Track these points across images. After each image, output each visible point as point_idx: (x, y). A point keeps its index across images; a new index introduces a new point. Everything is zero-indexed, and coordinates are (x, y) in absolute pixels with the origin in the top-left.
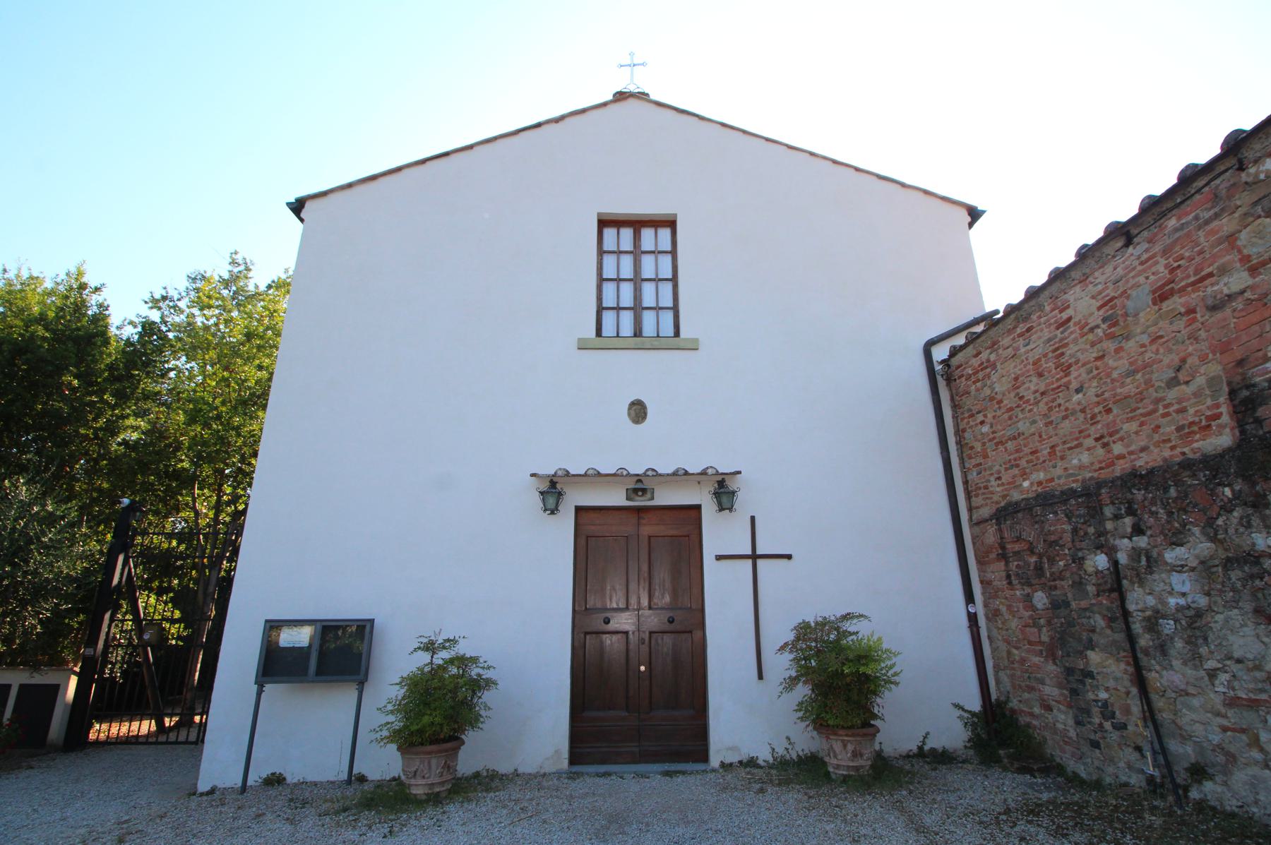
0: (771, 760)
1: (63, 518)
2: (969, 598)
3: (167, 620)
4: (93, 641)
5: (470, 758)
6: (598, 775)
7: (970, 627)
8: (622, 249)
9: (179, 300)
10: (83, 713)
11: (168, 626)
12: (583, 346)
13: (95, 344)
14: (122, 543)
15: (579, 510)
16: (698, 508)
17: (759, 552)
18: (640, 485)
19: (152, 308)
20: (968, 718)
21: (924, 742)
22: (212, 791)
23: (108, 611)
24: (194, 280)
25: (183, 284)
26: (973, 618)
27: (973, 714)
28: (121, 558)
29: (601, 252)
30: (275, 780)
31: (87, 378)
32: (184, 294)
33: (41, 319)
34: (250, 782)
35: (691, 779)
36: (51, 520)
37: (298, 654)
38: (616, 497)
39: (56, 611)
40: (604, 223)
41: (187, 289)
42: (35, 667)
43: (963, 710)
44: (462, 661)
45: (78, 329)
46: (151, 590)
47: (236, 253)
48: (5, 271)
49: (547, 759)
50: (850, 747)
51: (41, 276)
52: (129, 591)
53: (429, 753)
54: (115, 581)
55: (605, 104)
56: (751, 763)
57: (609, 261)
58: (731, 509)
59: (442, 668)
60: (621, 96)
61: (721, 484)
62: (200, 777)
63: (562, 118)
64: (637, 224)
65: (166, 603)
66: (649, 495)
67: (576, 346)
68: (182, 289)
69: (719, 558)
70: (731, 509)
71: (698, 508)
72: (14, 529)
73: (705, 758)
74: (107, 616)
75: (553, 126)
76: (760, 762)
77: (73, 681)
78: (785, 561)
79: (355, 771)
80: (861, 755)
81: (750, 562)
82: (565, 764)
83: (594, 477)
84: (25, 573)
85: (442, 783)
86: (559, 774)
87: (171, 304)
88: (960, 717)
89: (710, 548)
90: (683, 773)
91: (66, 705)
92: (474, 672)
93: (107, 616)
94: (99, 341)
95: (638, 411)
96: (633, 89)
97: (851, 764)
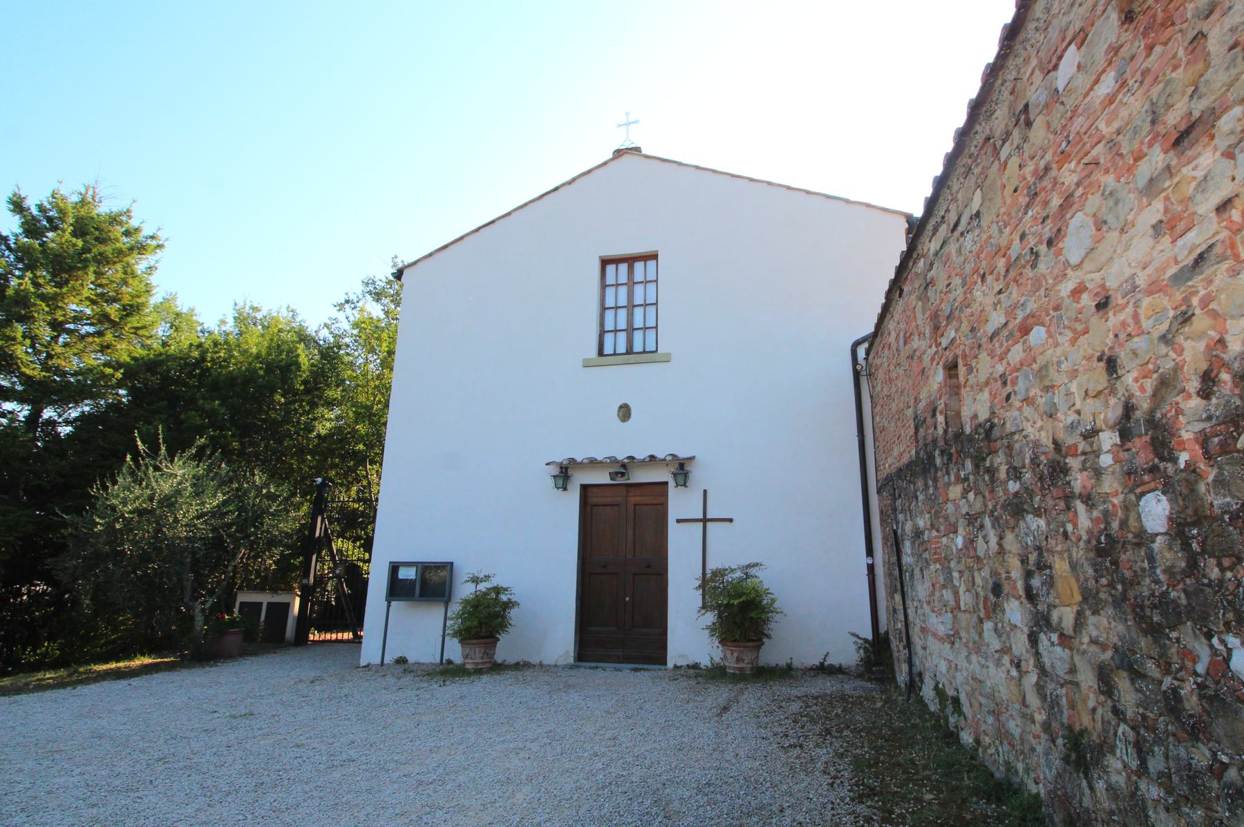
0: (710, 665)
1: (279, 496)
2: (870, 552)
3: (361, 560)
4: (307, 575)
5: (504, 650)
6: (590, 668)
7: (868, 575)
8: (619, 282)
9: (358, 302)
10: (304, 623)
11: (361, 564)
12: (587, 364)
13: (292, 370)
14: (319, 507)
15: (585, 488)
16: (666, 483)
17: (709, 516)
18: (623, 467)
19: (339, 310)
20: (861, 644)
21: (825, 660)
22: (368, 666)
23: (313, 554)
24: (367, 284)
25: (359, 288)
26: (871, 569)
27: (866, 641)
28: (319, 519)
29: (604, 286)
30: (402, 661)
31: (289, 391)
32: (361, 297)
33: (258, 356)
34: (385, 662)
35: (646, 674)
36: (272, 497)
37: (409, 584)
38: (602, 478)
39: (282, 554)
40: (605, 262)
41: (363, 291)
42: (274, 590)
43: (858, 636)
44: (498, 590)
45: (280, 361)
46: (344, 537)
47: (396, 257)
48: (236, 304)
49: (561, 656)
50: (735, 654)
51: (259, 306)
52: (326, 541)
53: (475, 644)
54: (317, 535)
55: (605, 163)
56: (695, 666)
57: (610, 292)
58: (685, 485)
59: (485, 594)
60: (619, 153)
61: (682, 466)
62: (362, 656)
63: (574, 180)
64: (631, 260)
65: (359, 548)
66: (626, 477)
67: (581, 364)
68: (359, 293)
69: (678, 521)
70: (685, 485)
71: (666, 483)
72: (254, 505)
73: (662, 660)
74: (314, 557)
75: (568, 187)
76: (702, 666)
77: (298, 600)
78: (727, 524)
79: (445, 657)
80: (743, 660)
81: (701, 524)
82: (571, 661)
83: (593, 463)
84: (262, 532)
85: (484, 663)
86: (565, 667)
87: (353, 306)
88: (855, 643)
89: (674, 512)
90: (645, 670)
91: (294, 617)
92: (504, 598)
93: (314, 557)
94: (293, 368)
95: (625, 412)
96: (628, 145)
97: (736, 666)
